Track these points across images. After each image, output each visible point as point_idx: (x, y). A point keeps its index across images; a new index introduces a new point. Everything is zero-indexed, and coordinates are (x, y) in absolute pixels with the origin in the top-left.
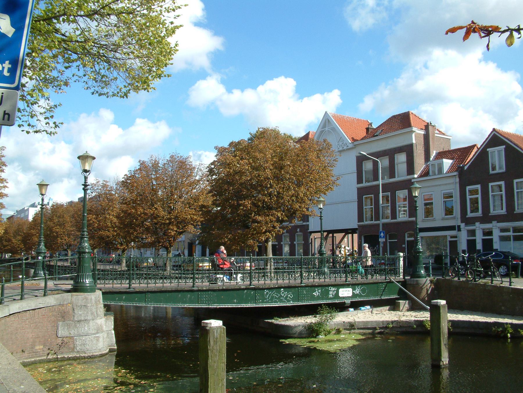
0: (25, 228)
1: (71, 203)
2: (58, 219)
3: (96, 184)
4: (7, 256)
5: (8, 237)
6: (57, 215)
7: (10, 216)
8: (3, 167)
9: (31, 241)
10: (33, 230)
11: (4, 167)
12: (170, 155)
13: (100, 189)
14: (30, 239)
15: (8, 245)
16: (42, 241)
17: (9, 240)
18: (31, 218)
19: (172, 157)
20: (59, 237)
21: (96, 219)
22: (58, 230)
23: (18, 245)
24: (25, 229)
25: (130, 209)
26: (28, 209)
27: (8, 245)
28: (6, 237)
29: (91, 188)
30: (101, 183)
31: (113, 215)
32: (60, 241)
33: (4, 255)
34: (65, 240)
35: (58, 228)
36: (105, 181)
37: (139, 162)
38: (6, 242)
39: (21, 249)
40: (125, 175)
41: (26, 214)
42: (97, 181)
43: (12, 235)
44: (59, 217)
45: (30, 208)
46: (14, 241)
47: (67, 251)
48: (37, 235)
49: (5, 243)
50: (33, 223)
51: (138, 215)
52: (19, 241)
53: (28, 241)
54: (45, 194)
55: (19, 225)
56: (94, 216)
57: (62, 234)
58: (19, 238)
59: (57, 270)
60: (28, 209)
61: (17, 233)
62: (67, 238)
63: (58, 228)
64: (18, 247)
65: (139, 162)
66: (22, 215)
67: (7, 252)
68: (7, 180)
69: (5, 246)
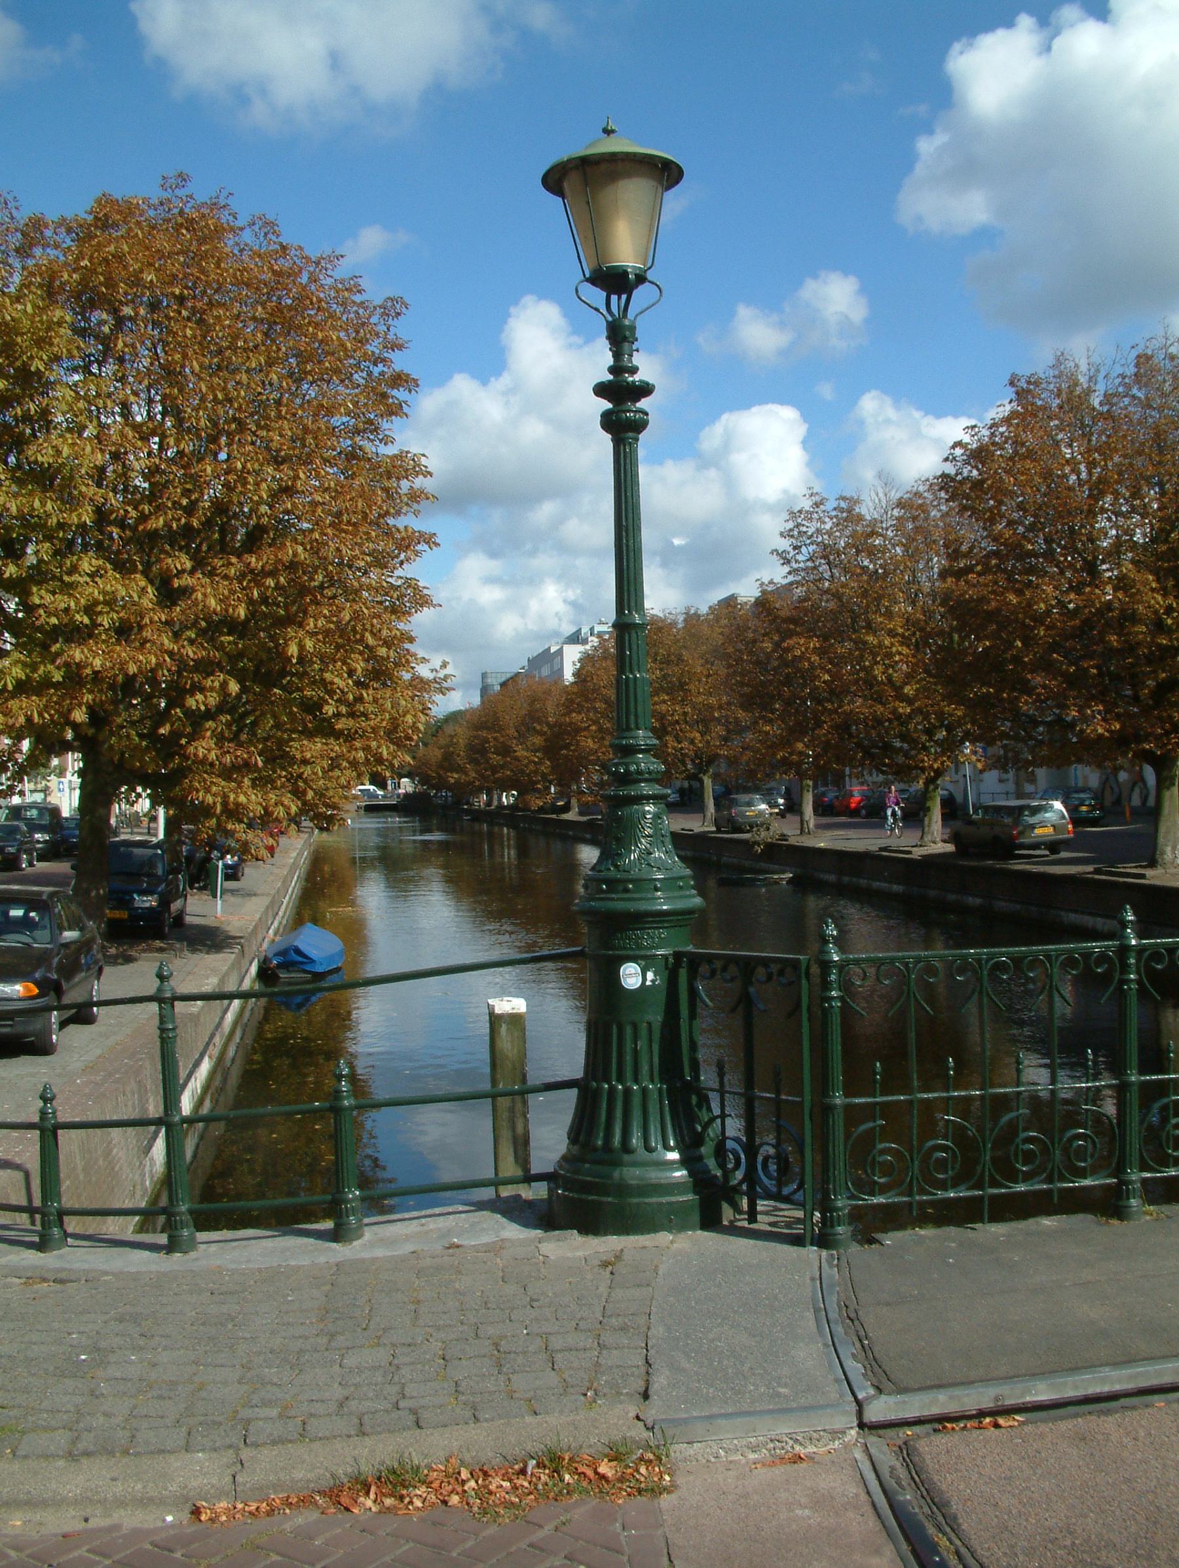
0: (550, 707)
1: (692, 619)
2: (661, 670)
3: (812, 513)
4: (504, 799)
5: (502, 740)
6: (656, 654)
7: (509, 676)
8: (395, 392)
9: (573, 751)
10: (580, 713)
11: (400, 394)
12: (1134, 353)
13: (830, 533)
14: (570, 744)
15: (502, 767)
16: (646, 789)
17: (505, 751)
18: (568, 676)
19: (1143, 360)
20: (667, 733)
21: (821, 652)
22: (664, 707)
23: (532, 767)
24: (552, 711)
25: (994, 592)
26: (560, 652)
27: (502, 767)
28: (495, 739)
29: (791, 530)
30: (830, 505)
31: (892, 633)
32: (674, 748)
33: (496, 797)
34: (692, 742)
35: (664, 702)
36: (844, 498)
37: (1012, 384)
38: (498, 754)
39: (544, 776)
40: (953, 447)
41: (556, 668)
42: (817, 498)
43: (512, 732)
44: (667, 662)
45: (566, 647)
46: (521, 752)
47: (701, 782)
48: (593, 728)
49: (495, 759)
50: (575, 690)
51: (1034, 619)
52: (536, 751)
53: (564, 752)
54: (641, 279)
55: (533, 700)
56: (814, 643)
57: (677, 722)
58: (538, 740)
59: (838, 1123)
60: (562, 648)
61: (531, 721)
62: (698, 735)
63: (664, 702)
64: (536, 772)
65: (1012, 384)
66: (545, 671)
67: (505, 786)
68: (423, 461)
69: (494, 769)
